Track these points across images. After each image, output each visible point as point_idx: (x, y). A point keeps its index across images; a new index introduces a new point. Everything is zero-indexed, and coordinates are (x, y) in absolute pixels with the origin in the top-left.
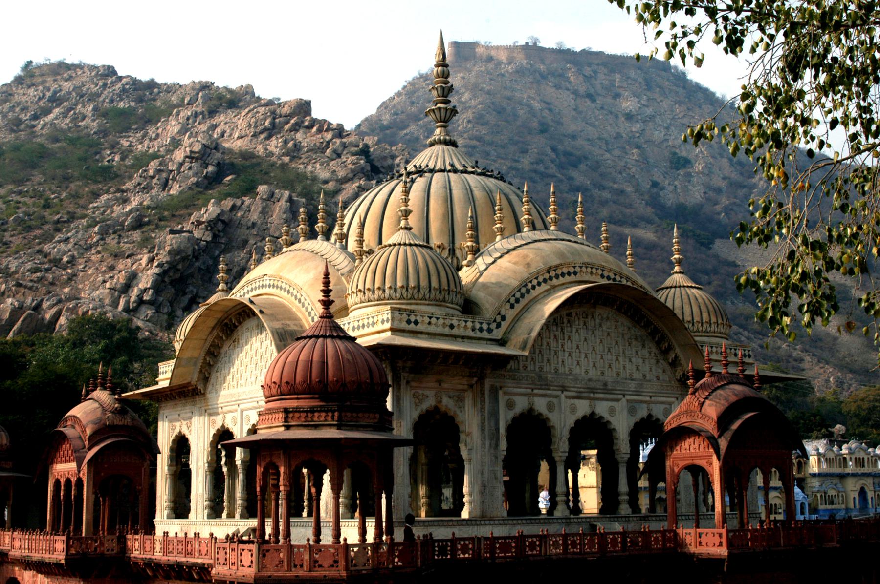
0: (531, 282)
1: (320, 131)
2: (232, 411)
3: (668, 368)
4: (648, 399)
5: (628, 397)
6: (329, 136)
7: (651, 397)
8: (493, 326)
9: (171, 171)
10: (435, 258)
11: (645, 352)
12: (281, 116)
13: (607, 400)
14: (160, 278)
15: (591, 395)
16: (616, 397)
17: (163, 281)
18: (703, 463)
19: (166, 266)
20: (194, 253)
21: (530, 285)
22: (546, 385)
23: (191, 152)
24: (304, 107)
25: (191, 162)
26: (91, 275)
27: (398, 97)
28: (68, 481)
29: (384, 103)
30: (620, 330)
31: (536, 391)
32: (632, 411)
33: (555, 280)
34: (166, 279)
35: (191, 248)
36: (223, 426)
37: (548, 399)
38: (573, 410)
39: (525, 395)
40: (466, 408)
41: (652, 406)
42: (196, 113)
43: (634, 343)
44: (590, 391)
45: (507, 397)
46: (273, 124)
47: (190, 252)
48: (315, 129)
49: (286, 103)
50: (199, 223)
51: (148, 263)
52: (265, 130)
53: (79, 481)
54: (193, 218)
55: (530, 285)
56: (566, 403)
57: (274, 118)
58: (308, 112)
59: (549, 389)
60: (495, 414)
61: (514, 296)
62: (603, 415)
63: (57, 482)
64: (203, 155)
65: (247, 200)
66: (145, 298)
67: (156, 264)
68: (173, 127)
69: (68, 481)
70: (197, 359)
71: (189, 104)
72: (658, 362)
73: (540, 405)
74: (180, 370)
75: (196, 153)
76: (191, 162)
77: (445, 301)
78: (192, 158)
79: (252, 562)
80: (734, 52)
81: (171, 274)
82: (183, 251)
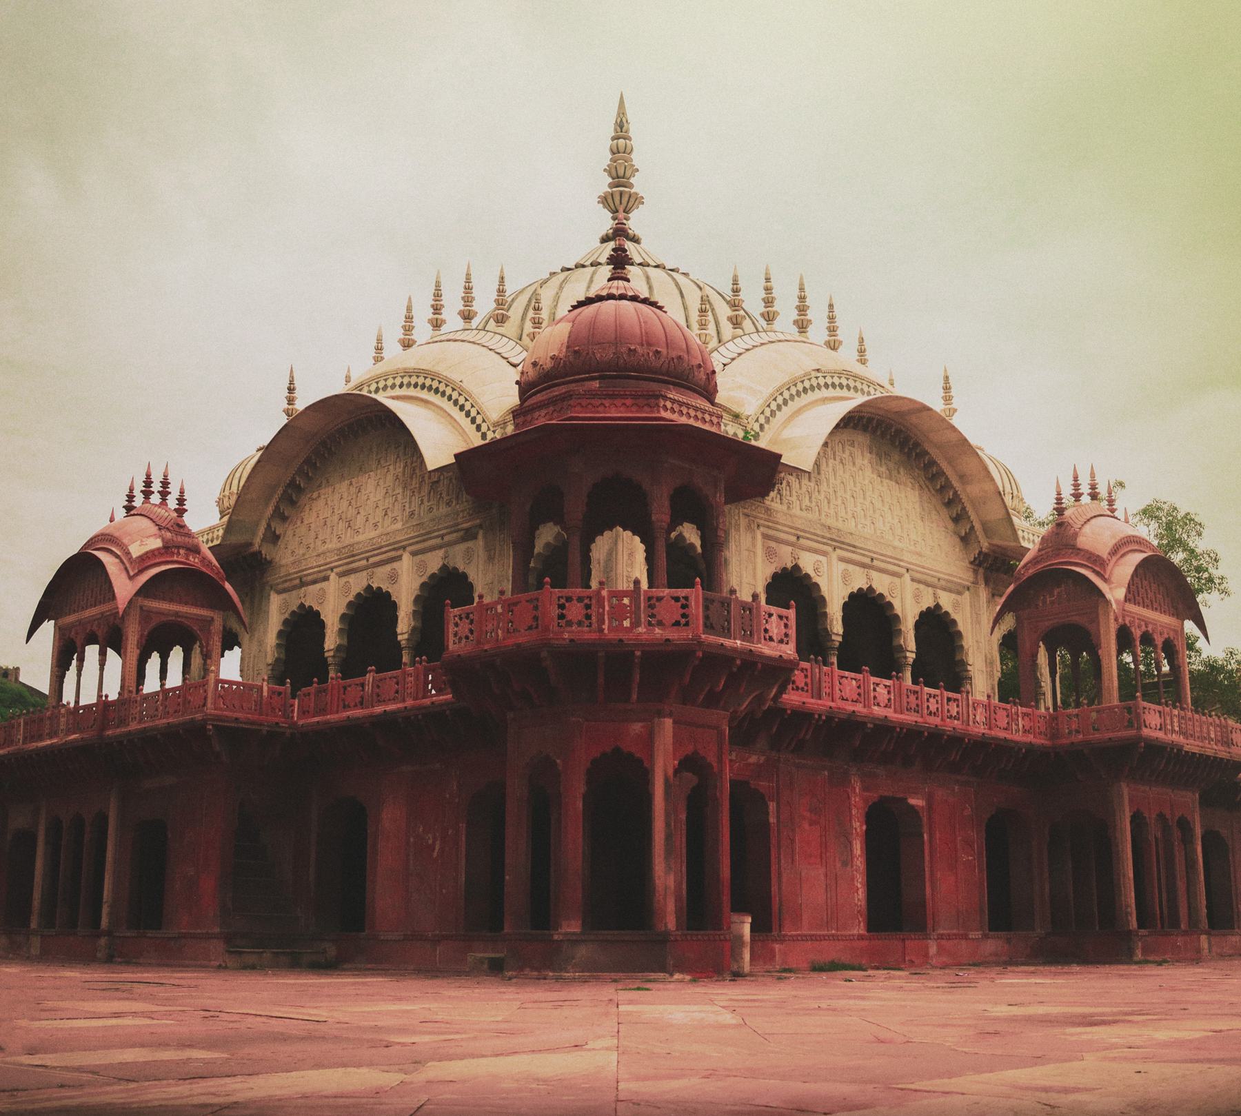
5: (839, 551)
39: (863, 566)
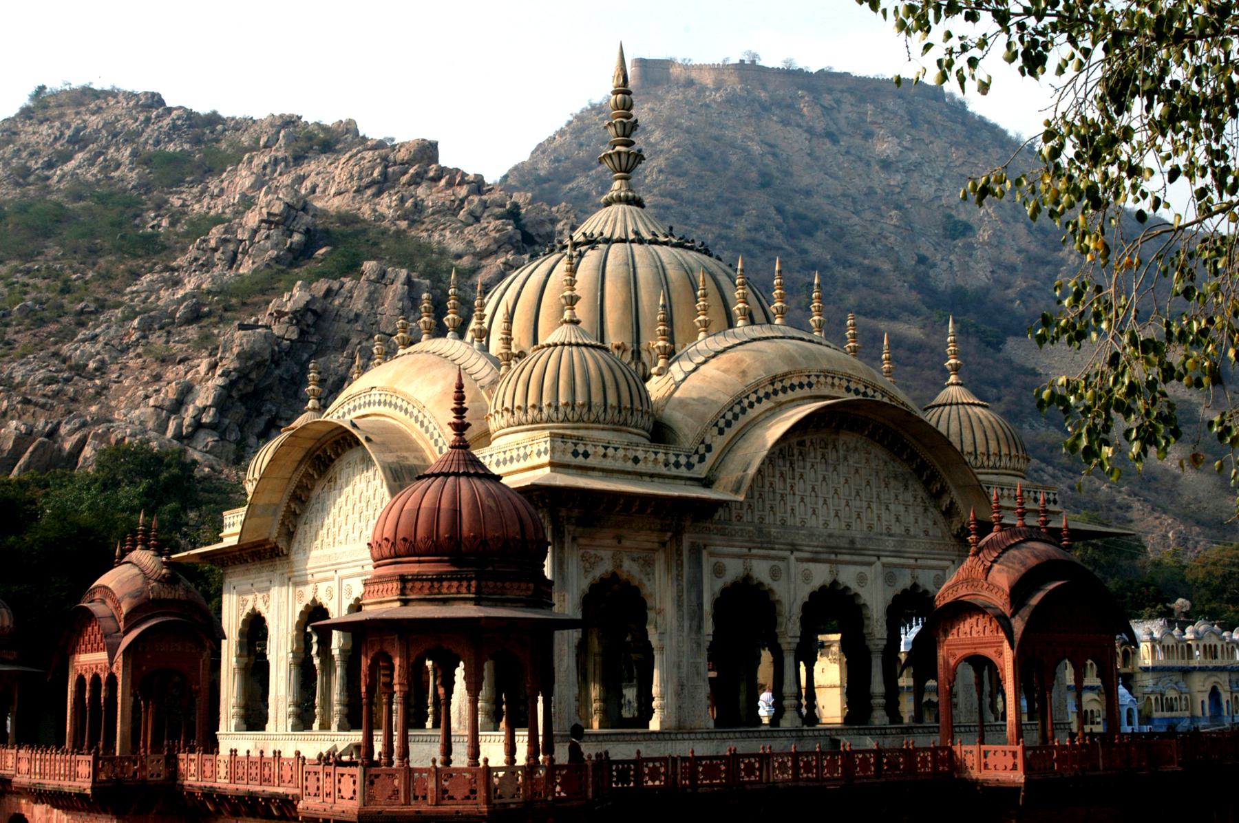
0: (747, 397)
1: (450, 184)
2: (326, 580)
3: (940, 518)
4: (912, 562)
5: (884, 560)
6: (463, 191)
7: (916, 559)
8: (695, 459)
9: (241, 241)
10: (612, 363)
11: (909, 496)
12: (395, 163)
13: (855, 563)
14: (225, 392)
15: (833, 556)
16: (867, 559)
17: (230, 396)
18: (989, 653)
19: (234, 375)
20: (273, 356)
21: (746, 402)
22: (769, 542)
23: (269, 214)
24: (427, 151)
25: (269, 229)
26: (129, 388)
27: (561, 136)
28: (96, 678)
29: (540, 145)
30: (873, 465)
31: (754, 551)
32: (890, 579)
33: (781, 395)
34: (234, 394)
35: (269, 350)
36: (314, 600)
37: (772, 563)
38: (807, 577)
39: (739, 556)
40: (657, 576)
41: (918, 572)
42: (276, 159)
43: (893, 483)
44: (831, 551)
45: (714, 560)
46: (384, 174)
47: (267, 356)
48: (443, 182)
49: (402, 145)
50: (280, 314)
51: (209, 370)
52: (373, 183)
53: (112, 678)
54: (271, 308)
55: (746, 402)
56: (797, 568)
57: (386, 167)
58: (434, 158)
59: (773, 549)
60: (697, 584)
61: (723, 417)
62: (849, 584)
63: (81, 679)
64: (286, 219)
65: (348, 282)
66: (204, 420)
67: (219, 371)
68: (243, 179)
69: (96, 678)
70: (277, 505)
71: (265, 146)
72: (926, 510)
73: (761, 571)
74: (254, 521)
75: (276, 215)
76: (269, 229)
77: (626, 425)
78: (270, 223)
79: (354, 792)
80: (1033, 73)
81: (241, 386)
82: (258, 354)
